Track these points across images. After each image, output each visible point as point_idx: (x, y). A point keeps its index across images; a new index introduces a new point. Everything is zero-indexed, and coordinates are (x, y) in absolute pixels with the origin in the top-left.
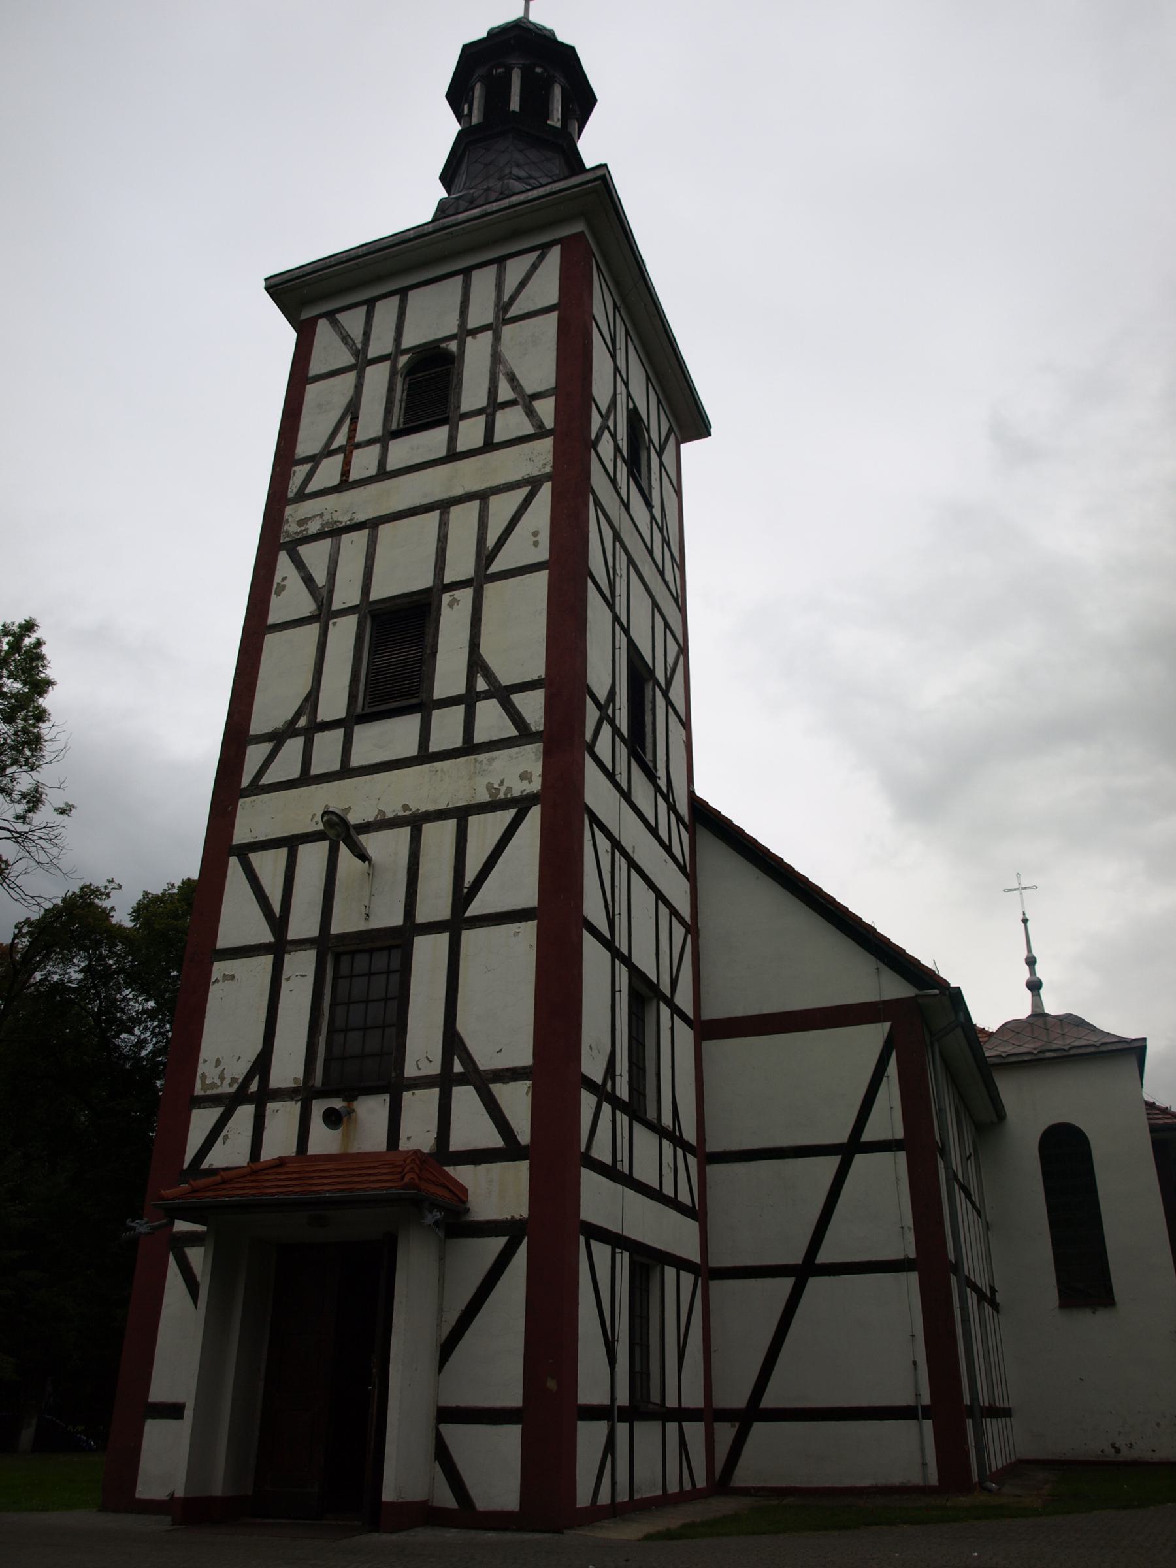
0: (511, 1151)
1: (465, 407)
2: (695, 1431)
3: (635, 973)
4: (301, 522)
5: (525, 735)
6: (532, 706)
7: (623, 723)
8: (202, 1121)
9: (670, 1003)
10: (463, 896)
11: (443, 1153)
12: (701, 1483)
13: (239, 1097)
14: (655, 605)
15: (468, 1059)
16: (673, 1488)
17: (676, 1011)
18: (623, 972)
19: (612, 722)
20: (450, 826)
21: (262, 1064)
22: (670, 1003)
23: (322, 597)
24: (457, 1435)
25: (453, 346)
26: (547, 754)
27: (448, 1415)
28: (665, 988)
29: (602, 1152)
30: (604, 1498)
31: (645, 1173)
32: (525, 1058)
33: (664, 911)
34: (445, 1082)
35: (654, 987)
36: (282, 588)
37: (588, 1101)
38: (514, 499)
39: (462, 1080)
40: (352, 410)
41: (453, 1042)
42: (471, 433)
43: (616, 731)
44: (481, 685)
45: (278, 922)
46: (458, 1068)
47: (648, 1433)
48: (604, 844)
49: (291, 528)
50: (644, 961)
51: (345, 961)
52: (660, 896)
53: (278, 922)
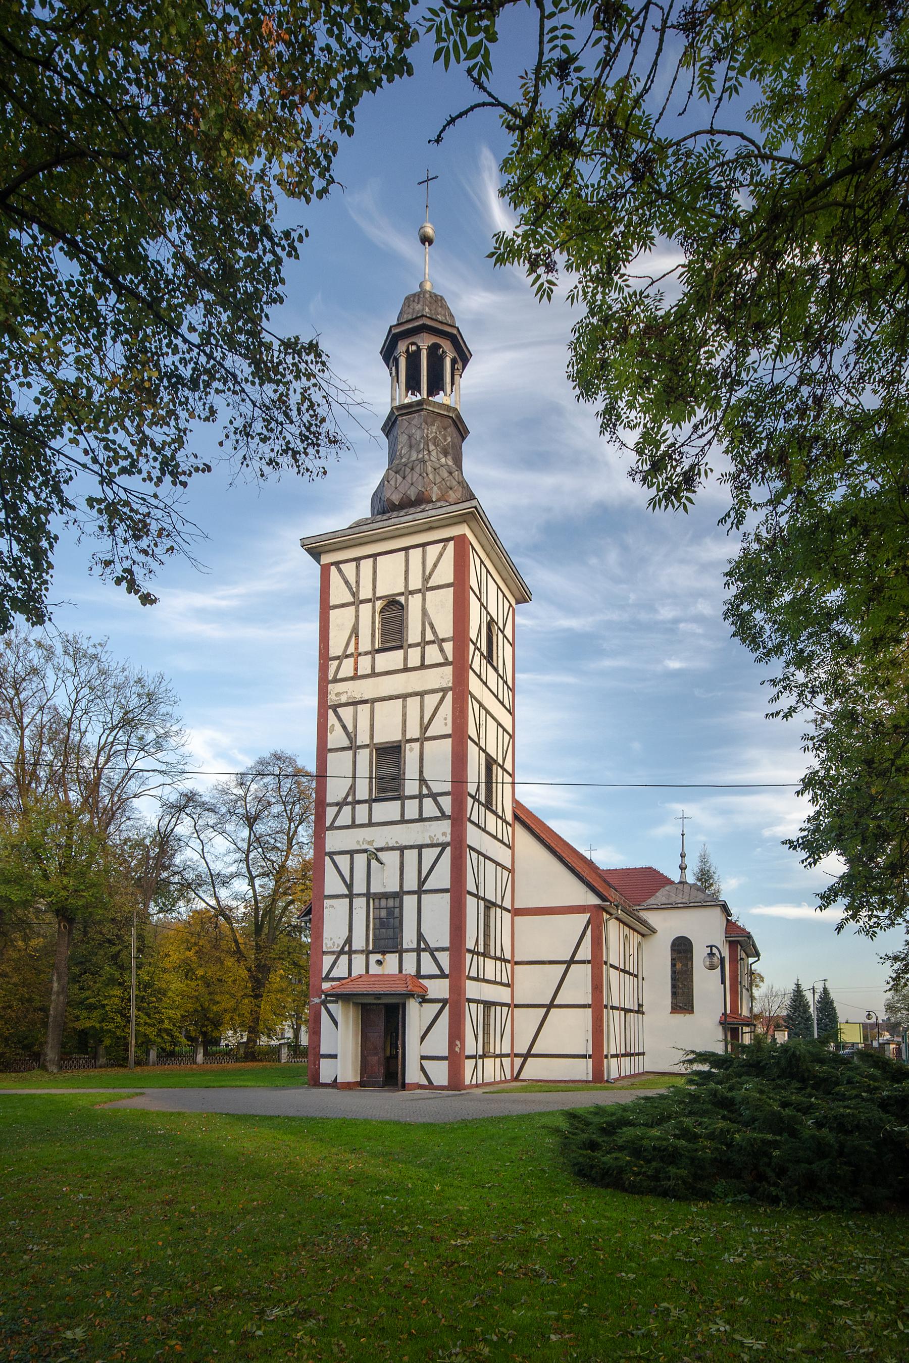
0: (443, 976)
1: (410, 641)
2: (506, 1061)
3: (487, 755)
4: (338, 694)
5: (444, 816)
6: (446, 803)
7: (484, 649)
8: (327, 961)
9: (502, 767)
10: (422, 883)
11: (419, 976)
12: (509, 1077)
13: (342, 952)
14: (499, 587)
15: (426, 943)
16: (498, 1079)
17: (504, 770)
18: (483, 755)
19: (479, 650)
20: (410, 665)
21: (349, 941)
22: (502, 767)
23: (351, 737)
24: (428, 1064)
25: (402, 599)
26: (453, 825)
27: (423, 1058)
28: (500, 761)
29: (474, 818)
30: (474, 1082)
31: (490, 976)
32: (447, 944)
33: (500, 730)
34: (418, 950)
35: (496, 762)
36: (332, 730)
37: (470, 801)
38: (435, 698)
39: (424, 950)
40: (355, 631)
41: (420, 937)
42: (414, 656)
43: (482, 654)
44: (425, 791)
45: (350, 886)
46: (423, 946)
47: (489, 1062)
48: (476, 706)
49: (332, 699)
50: (492, 752)
51: (377, 901)
52: (499, 724)
53: (350, 886)
